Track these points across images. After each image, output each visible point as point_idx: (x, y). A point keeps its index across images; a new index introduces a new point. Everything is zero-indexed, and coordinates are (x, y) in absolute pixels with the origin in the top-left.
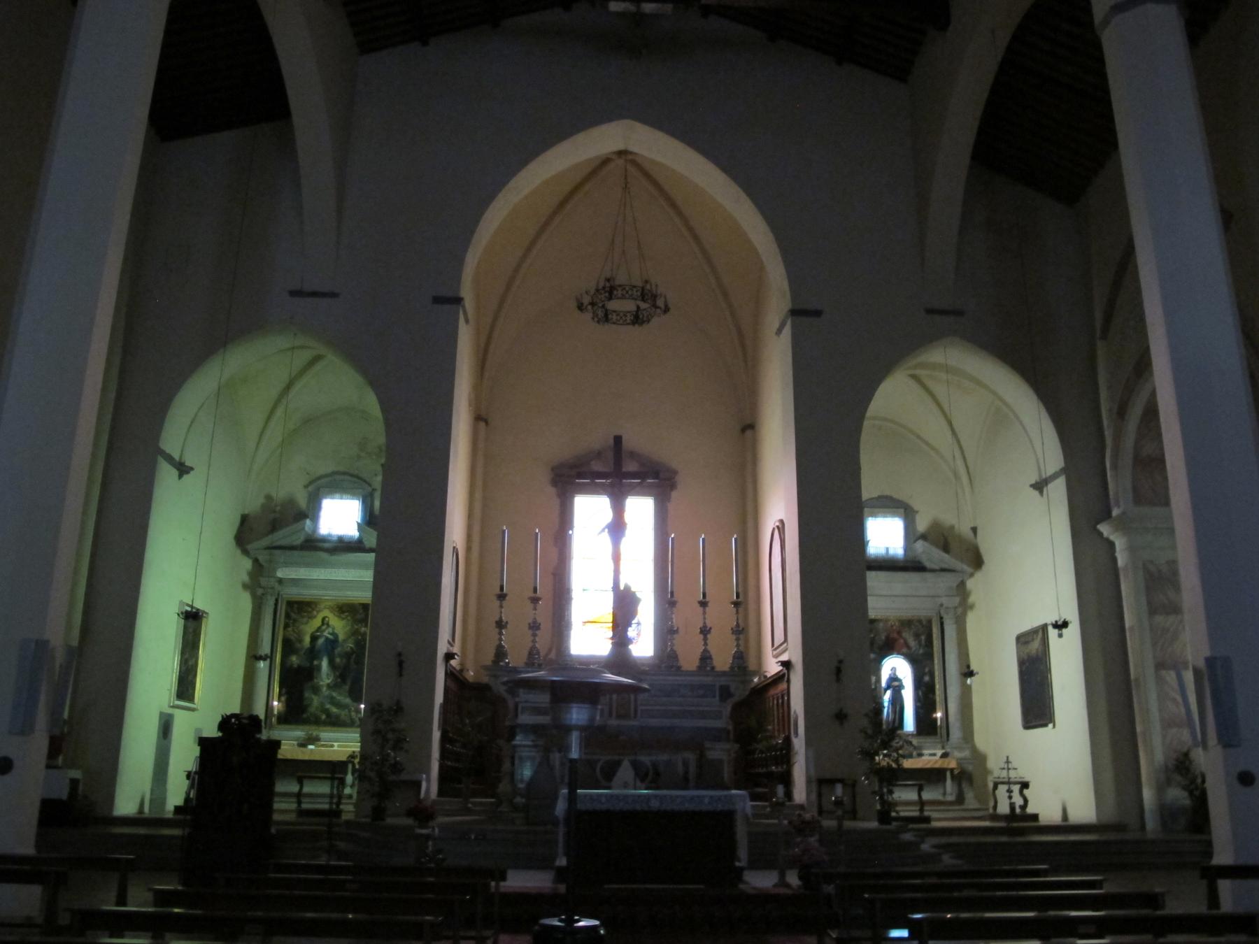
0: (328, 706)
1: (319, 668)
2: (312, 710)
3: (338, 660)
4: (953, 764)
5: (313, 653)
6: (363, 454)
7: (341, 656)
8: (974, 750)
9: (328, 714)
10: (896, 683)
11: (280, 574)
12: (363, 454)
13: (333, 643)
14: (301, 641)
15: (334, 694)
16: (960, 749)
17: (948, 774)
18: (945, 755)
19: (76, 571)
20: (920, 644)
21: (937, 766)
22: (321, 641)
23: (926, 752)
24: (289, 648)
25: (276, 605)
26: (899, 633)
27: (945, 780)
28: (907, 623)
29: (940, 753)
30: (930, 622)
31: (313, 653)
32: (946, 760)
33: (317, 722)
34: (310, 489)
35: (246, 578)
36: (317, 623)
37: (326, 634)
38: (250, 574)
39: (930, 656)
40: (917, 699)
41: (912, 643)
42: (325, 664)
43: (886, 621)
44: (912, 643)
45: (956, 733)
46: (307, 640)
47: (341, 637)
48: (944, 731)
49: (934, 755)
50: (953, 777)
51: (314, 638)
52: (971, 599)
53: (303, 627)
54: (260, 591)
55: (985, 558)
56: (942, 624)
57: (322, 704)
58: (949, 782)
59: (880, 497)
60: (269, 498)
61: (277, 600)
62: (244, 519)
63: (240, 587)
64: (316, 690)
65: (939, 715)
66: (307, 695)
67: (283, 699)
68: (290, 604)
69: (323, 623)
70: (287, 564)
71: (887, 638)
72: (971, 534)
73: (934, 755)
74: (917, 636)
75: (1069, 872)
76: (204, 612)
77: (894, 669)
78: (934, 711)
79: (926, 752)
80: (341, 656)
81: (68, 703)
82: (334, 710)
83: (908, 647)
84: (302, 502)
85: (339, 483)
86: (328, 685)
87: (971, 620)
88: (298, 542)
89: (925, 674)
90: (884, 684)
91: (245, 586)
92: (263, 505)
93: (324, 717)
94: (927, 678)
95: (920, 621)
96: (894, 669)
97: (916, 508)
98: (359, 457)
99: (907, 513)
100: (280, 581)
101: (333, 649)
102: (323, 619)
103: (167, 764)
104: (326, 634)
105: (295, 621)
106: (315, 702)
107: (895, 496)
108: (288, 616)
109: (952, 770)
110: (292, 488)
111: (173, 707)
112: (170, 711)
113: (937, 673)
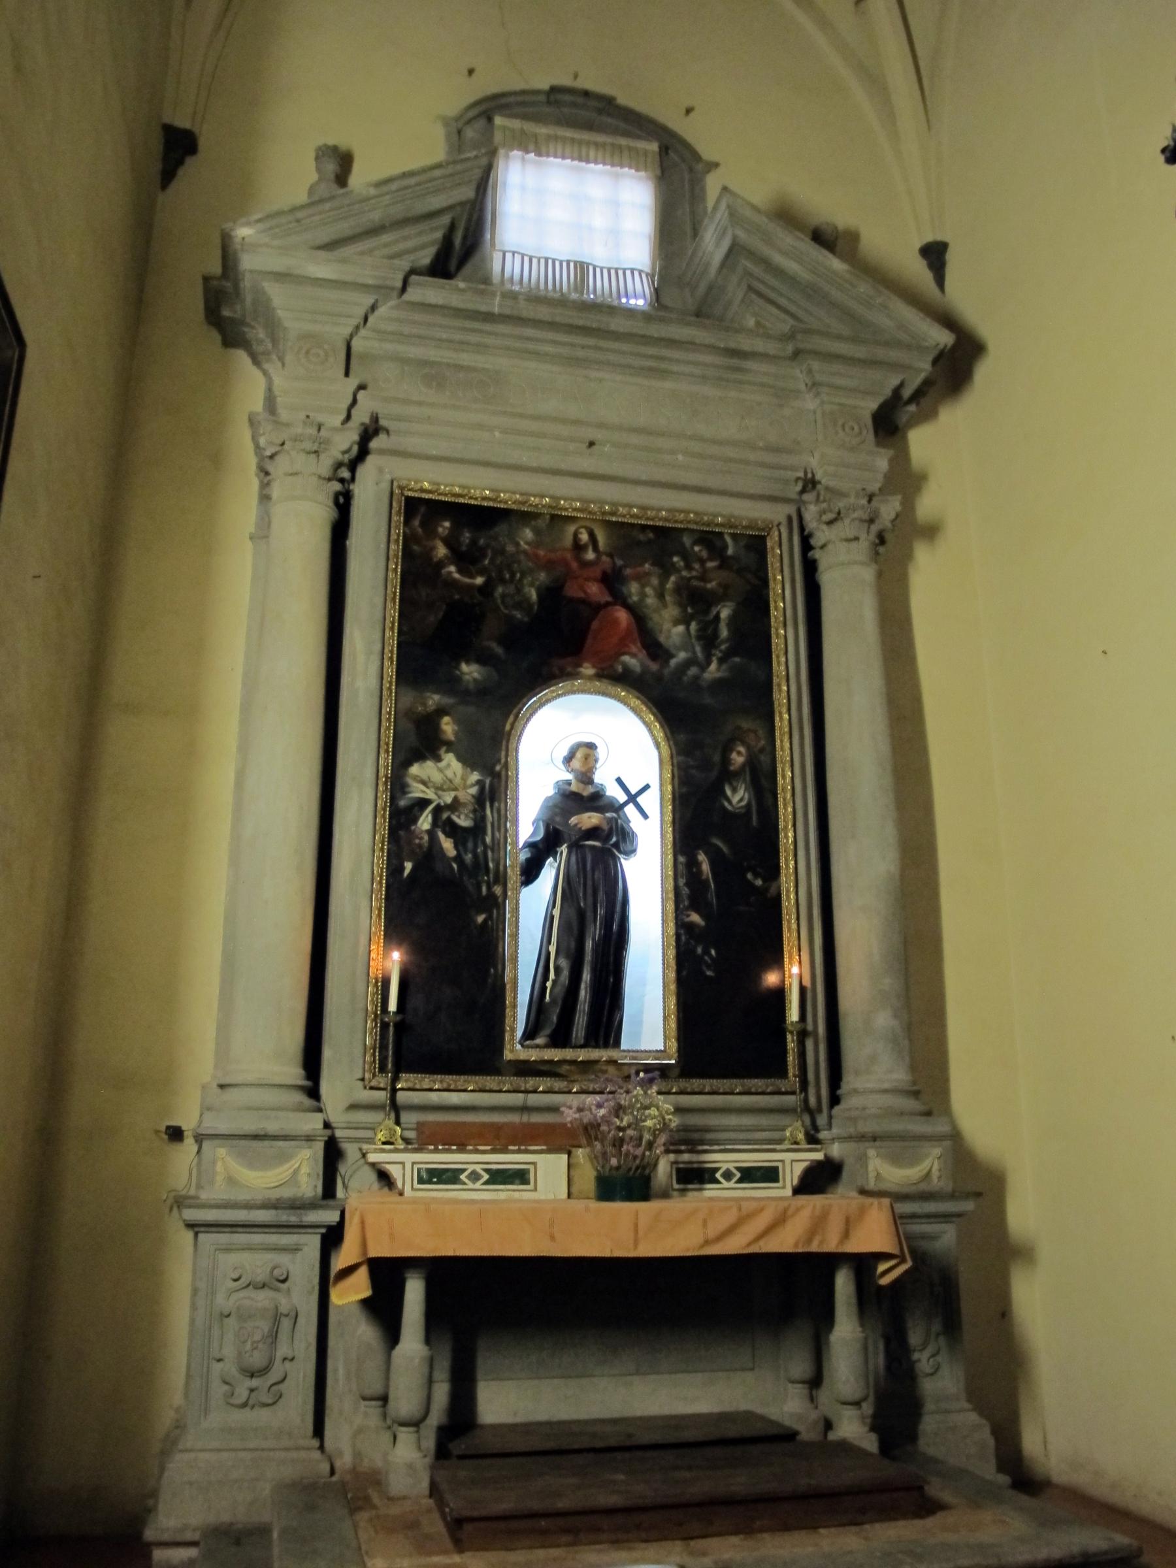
4: (874, 1234)
8: (960, 1155)
10: (590, 819)
16: (900, 1144)
17: (843, 1283)
18: (821, 1178)
19: (744, 1189)
20: (708, 638)
21: (784, 1242)
23: (722, 1160)
26: (612, 581)
27: (825, 1317)
28: (652, 542)
29: (794, 1163)
30: (756, 544)
32: (838, 1201)
39: (757, 696)
40: (687, 891)
41: (673, 631)
43: (558, 520)
44: (673, 631)
45: (874, 1067)
48: (816, 1052)
49: (770, 1175)
50: (869, 1296)
52: (927, 505)
55: (835, 1426)
56: (810, 568)
58: (846, 1329)
59: (554, 90)
63: (1045, 1252)
65: (794, 971)
71: (552, 594)
72: (918, 272)
73: (770, 1175)
74: (696, 602)
75: (6, 386)
77: (583, 755)
78: (775, 957)
79: (722, 1160)
83: (656, 650)
87: (927, 573)
89: (727, 775)
90: (527, 824)
94: (738, 797)
95: (710, 539)
96: (583, 755)
97: (707, 152)
99: (677, 171)
107: (622, 100)
109: (863, 1264)
113: (785, 776)
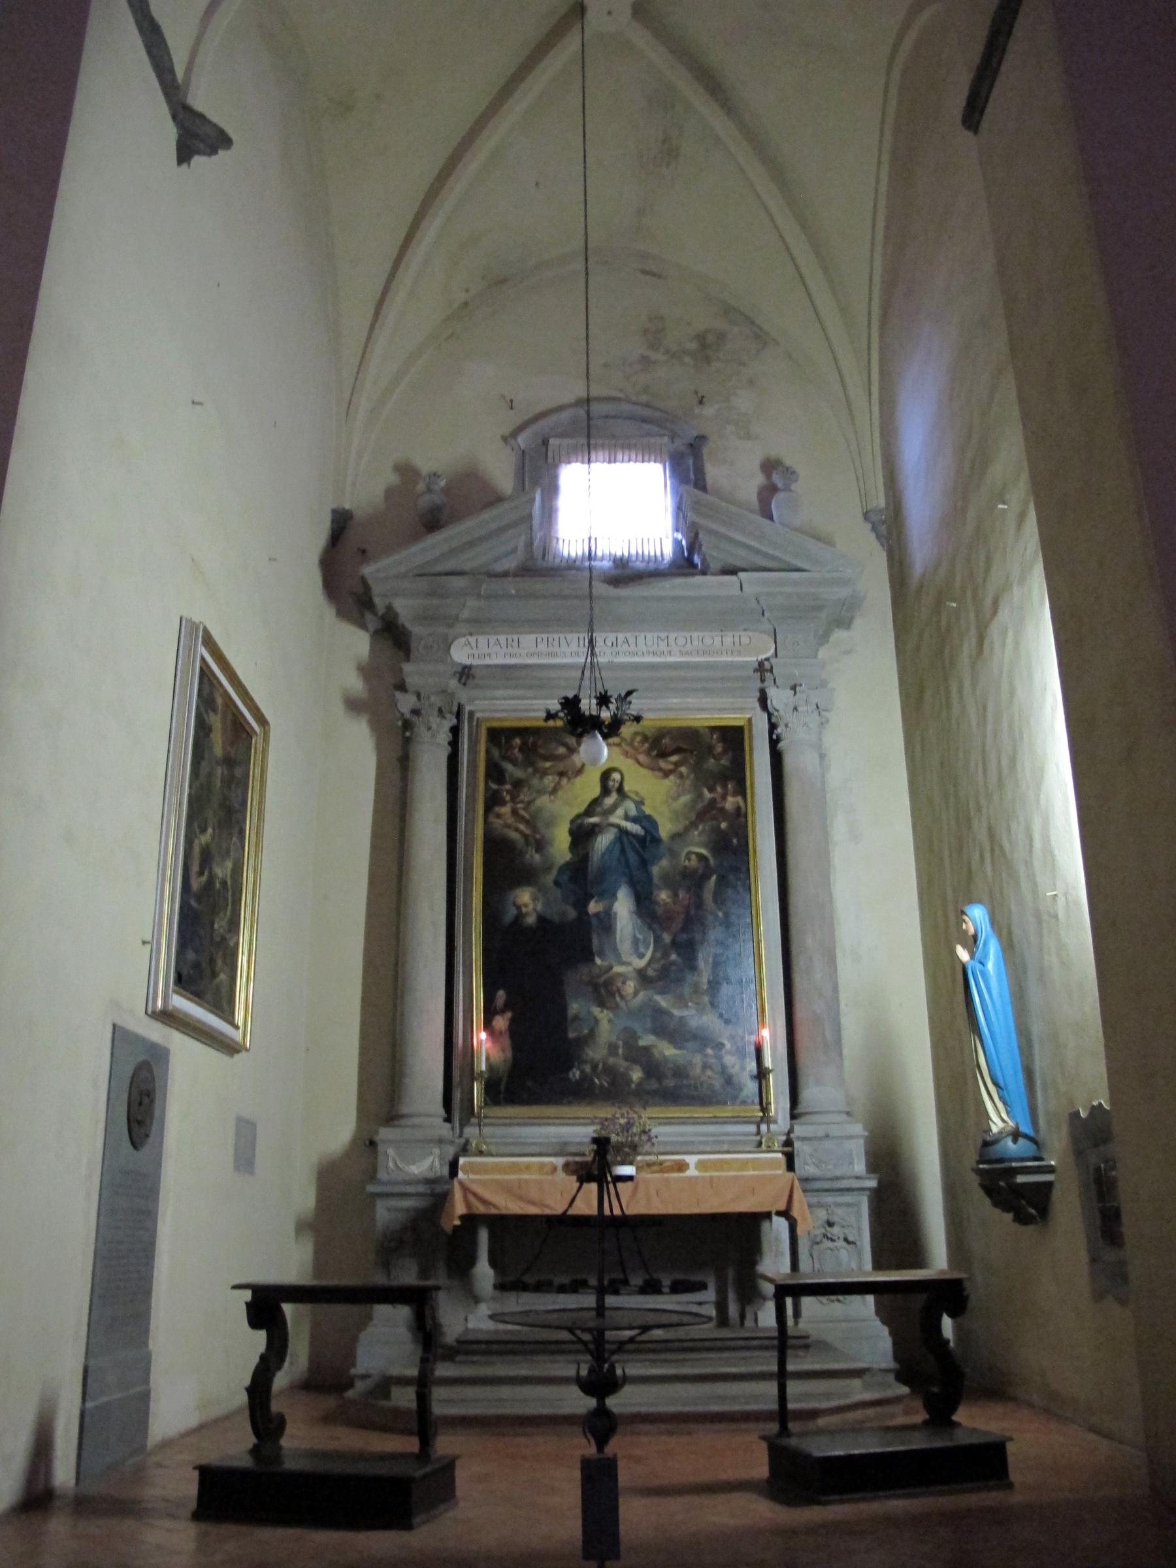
0: (647, 1040)
1: (607, 922)
2: (596, 1053)
3: (663, 896)
5: (581, 878)
6: (659, 356)
7: (669, 881)
9: (653, 1069)
11: (461, 654)
12: (654, 356)
13: (643, 844)
14: (541, 845)
15: (663, 1002)
22: (604, 841)
24: (506, 864)
25: (454, 744)
31: (581, 878)
33: (615, 1091)
34: (522, 440)
35: (356, 684)
36: (587, 788)
37: (617, 818)
38: (367, 671)
42: (623, 906)
46: (561, 843)
47: (665, 830)
51: (582, 835)
53: (543, 801)
54: (406, 703)
57: (630, 1038)
60: (406, 471)
61: (455, 731)
62: (341, 524)
63: (339, 708)
64: (604, 991)
66: (575, 1007)
67: (501, 1022)
68: (498, 736)
69: (606, 791)
70: (481, 624)
76: (334, 511)
80: (669, 881)
81: (499, 1177)
82: (667, 1051)
84: (500, 470)
85: (597, 428)
86: (641, 974)
88: (509, 564)
91: (353, 705)
92: (389, 493)
93: (636, 1075)
98: (645, 361)
100: (465, 674)
101: (644, 864)
102: (606, 776)
103: (146, 1252)
104: (617, 818)
105: (518, 784)
106: (604, 1029)
108: (495, 773)
110: (464, 437)
111: (168, 1017)
112: (156, 1033)
